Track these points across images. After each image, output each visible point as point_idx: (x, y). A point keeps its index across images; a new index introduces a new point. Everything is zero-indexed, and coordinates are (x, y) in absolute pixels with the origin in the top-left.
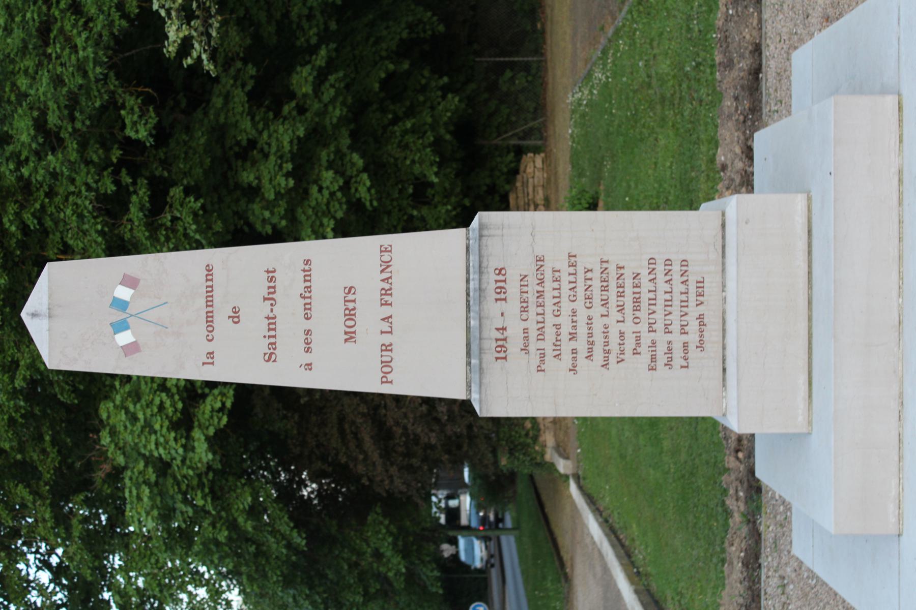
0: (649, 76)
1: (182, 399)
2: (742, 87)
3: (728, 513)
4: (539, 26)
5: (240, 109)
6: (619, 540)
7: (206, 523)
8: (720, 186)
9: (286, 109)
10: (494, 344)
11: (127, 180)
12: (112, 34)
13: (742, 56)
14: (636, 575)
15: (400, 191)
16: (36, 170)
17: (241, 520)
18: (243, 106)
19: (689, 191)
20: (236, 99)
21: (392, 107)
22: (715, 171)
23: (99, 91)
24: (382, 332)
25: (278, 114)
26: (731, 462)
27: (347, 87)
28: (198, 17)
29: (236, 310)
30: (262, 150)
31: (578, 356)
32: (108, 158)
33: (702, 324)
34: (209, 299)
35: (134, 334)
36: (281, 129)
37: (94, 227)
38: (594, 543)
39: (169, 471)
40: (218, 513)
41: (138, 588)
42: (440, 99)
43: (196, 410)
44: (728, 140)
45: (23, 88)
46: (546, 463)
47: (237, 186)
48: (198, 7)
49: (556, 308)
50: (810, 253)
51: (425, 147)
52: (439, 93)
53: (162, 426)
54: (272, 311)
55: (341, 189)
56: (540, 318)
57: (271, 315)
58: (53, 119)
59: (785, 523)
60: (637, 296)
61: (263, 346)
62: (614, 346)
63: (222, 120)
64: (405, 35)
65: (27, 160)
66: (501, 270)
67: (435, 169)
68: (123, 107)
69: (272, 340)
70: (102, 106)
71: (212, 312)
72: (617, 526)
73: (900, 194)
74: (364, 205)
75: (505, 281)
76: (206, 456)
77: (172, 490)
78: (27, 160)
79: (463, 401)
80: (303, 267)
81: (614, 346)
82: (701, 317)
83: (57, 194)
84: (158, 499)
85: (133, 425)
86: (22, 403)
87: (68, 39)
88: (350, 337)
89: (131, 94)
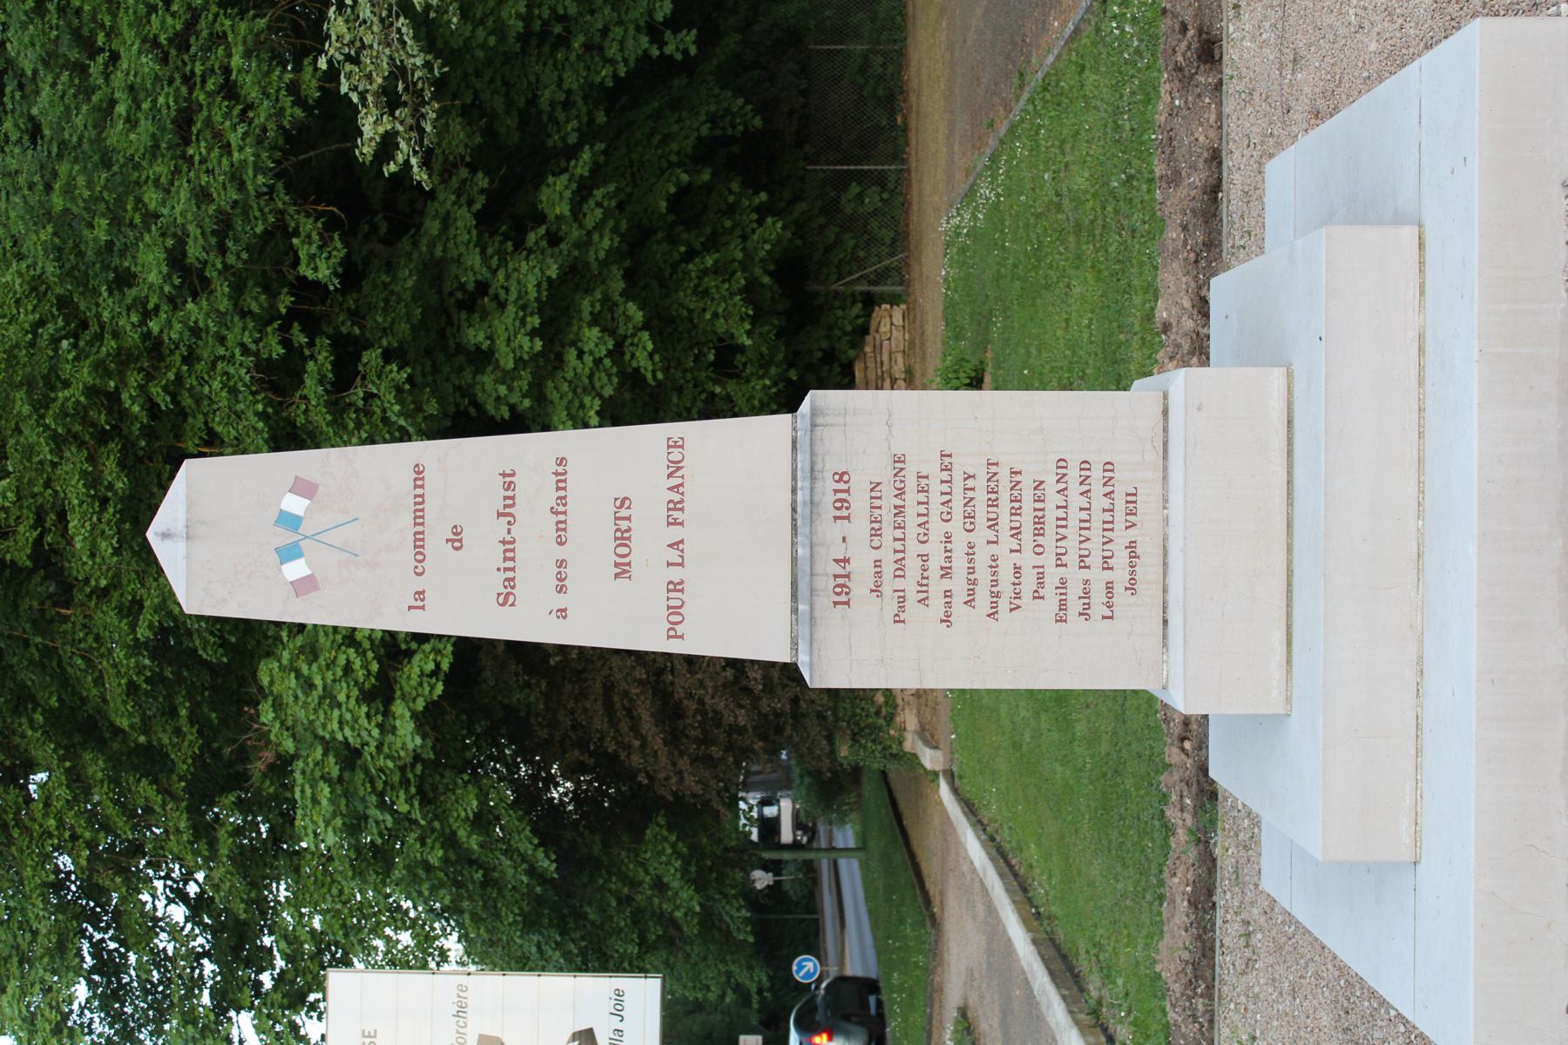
0: (1058, 194)
1: (378, 658)
2: (1193, 211)
3: (1168, 829)
6: (1010, 866)
7: (411, 838)
9: (532, 238)
10: (832, 583)
17: (462, 833)
18: (469, 233)
20: (460, 223)
21: (685, 236)
23: (261, 210)
24: (669, 564)
25: (519, 245)
27: (621, 206)
29: (457, 531)
30: (496, 297)
31: (954, 600)
32: (273, 306)
33: (1134, 555)
34: (418, 514)
35: (309, 564)
36: (524, 267)
38: (974, 870)
39: (359, 762)
40: (430, 823)
42: (755, 225)
43: (398, 674)
44: (1173, 289)
45: (152, 206)
46: (906, 753)
48: (406, 89)
49: (922, 531)
50: (1290, 453)
51: (732, 294)
52: (754, 216)
53: (348, 697)
54: (509, 531)
56: (898, 545)
57: (508, 538)
58: (194, 251)
60: (1040, 514)
61: (497, 583)
62: (1006, 587)
63: (439, 252)
64: (705, 131)
65: (157, 308)
68: (296, 233)
69: (510, 574)
70: (266, 232)
71: (422, 533)
75: (847, 491)
76: (413, 740)
78: (157, 308)
80: (555, 468)
81: (1006, 587)
82: (1132, 546)
84: (343, 802)
85: (307, 695)
86: (147, 662)
88: (622, 570)
89: (308, 215)
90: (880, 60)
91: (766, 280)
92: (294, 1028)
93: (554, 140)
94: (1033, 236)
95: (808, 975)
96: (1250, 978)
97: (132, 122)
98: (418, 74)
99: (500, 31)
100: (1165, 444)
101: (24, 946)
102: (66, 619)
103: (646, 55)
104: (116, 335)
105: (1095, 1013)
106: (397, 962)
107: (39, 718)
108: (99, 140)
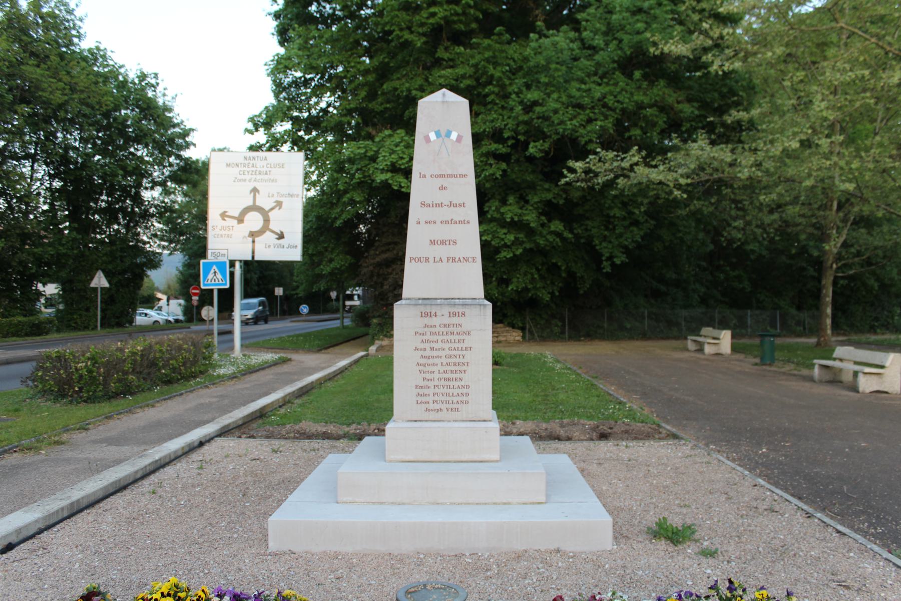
0: (558, 389)
3: (349, 425)
4: (582, 338)
8: (505, 422)
9: (543, 218)
10: (428, 311)
11: (510, 143)
12: (578, 137)
13: (566, 432)
14: (320, 383)
15: (504, 272)
16: (514, 101)
17: (348, 196)
19: (503, 407)
21: (544, 268)
22: (512, 420)
25: (541, 214)
26: (373, 426)
27: (554, 247)
28: (586, 176)
32: (520, 134)
33: (438, 411)
37: (488, 127)
41: (317, 148)
47: (507, 195)
50: (471, 462)
51: (525, 283)
55: (505, 243)
56: (441, 333)
58: (538, 109)
59: (344, 451)
61: (429, 201)
62: (427, 368)
64: (578, 275)
65: (519, 97)
67: (515, 289)
72: (343, 374)
73: (499, 504)
74: (498, 254)
77: (363, 163)
78: (519, 97)
79: (401, 295)
81: (427, 368)
82: (441, 410)
84: (358, 157)
87: (575, 117)
88: (433, 242)
91: (530, 295)
92: (286, 142)
96: (300, 451)
98: (596, 181)
99: (610, 208)
102: (418, 68)
104: (511, 84)
105: (289, 402)
106: (307, 175)
107: (386, 60)
108: (573, 79)
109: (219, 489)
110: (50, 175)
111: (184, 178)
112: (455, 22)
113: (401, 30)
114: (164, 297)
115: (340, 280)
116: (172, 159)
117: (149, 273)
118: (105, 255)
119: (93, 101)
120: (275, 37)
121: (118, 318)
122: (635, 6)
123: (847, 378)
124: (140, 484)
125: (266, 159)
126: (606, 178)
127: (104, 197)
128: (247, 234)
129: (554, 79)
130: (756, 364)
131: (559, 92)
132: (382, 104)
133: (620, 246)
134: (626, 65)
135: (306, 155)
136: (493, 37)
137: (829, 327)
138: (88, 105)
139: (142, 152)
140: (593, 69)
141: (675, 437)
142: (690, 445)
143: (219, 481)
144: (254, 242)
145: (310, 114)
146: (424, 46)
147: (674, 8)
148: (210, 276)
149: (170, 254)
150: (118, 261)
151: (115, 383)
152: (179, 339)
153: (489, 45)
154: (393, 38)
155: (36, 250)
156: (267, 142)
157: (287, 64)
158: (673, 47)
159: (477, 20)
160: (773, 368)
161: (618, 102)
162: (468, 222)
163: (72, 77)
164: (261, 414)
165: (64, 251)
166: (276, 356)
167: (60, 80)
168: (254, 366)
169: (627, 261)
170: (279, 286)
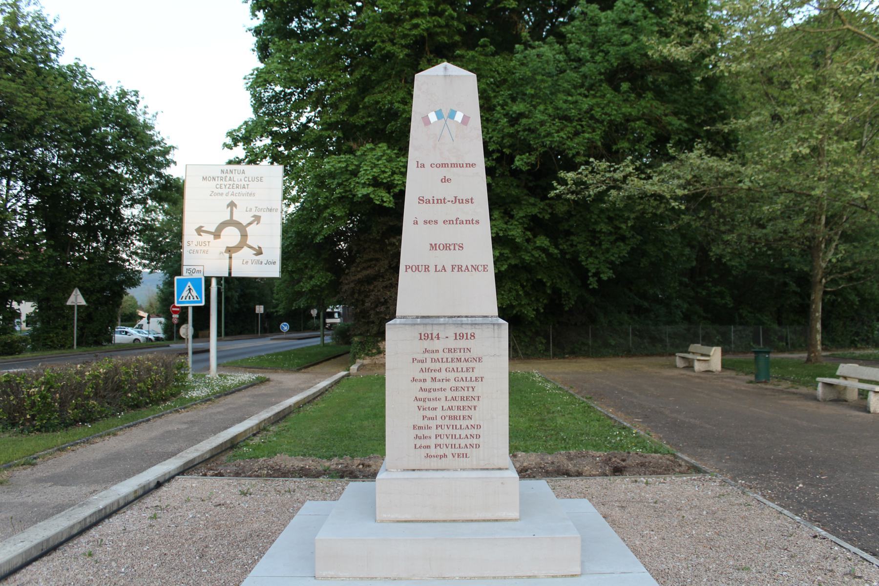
0: (553, 412)
1: (388, 182)
2: (559, 466)
3: (329, 458)
5: (529, 211)
6: (317, 397)
7: (327, 194)
9: (528, 233)
10: (429, 332)
14: (299, 406)
16: (499, 113)
17: (329, 211)
21: (529, 285)
25: (526, 229)
27: (539, 263)
29: (449, 180)
30: (509, 221)
31: (422, 383)
32: (505, 147)
33: (441, 457)
36: (519, 231)
38: (316, 384)
40: (332, 200)
45: (539, 108)
48: (582, 189)
49: (451, 369)
50: (484, 521)
51: (510, 300)
56: (445, 360)
57: (446, 201)
58: (524, 121)
63: (523, 202)
64: (563, 291)
66: (474, 336)
69: (431, 201)
70: (530, 144)
73: (522, 577)
75: (467, 339)
77: (344, 178)
78: (504, 109)
80: (475, 220)
82: (445, 456)
83: (488, 123)
84: (339, 171)
85: (375, 159)
88: (433, 247)
90: (586, 349)
91: (515, 312)
92: (265, 157)
93: (560, 241)
94: (536, 403)
95: (283, 328)
96: (273, 493)
97: (566, 102)
98: (587, 193)
99: (596, 223)
100: (487, 469)
101: (293, 70)
102: (401, 81)
103: (589, 271)
104: (495, 97)
105: (264, 429)
106: (286, 191)
107: (368, 73)
108: (559, 92)
109: (172, 548)
110: (27, 192)
111: (164, 195)
112: (438, 34)
113: (383, 42)
114: (146, 315)
115: (320, 298)
116: (152, 177)
117: (128, 290)
118: (84, 272)
119: (70, 116)
120: (256, 53)
121: (96, 336)
122: (620, 19)
123: (853, 396)
124: (75, 542)
125: (243, 172)
126: (598, 189)
127: (83, 215)
128: (224, 249)
129: (540, 90)
130: (751, 382)
131: (545, 103)
132: (363, 117)
133: (607, 261)
134: (612, 78)
135: (285, 170)
136: (479, 49)
137: (819, 343)
138: (65, 121)
139: (122, 170)
140: (580, 81)
141: (698, 470)
142: (718, 480)
143: (173, 536)
144: (230, 258)
145: (290, 129)
146: (407, 58)
147: (660, 20)
148: (185, 293)
149: (151, 272)
150: (97, 279)
151: (73, 410)
152: (148, 360)
153: (473, 56)
154: (375, 49)
155: (10, 268)
156: (246, 157)
157: (267, 78)
158: (673, 49)
159: (460, 32)
160: (768, 386)
161: (606, 114)
162: (477, 222)
163: (49, 92)
164: (232, 445)
165: (40, 269)
166: (254, 377)
167: (36, 95)
168: (230, 387)
169: (614, 276)
170: (260, 304)
